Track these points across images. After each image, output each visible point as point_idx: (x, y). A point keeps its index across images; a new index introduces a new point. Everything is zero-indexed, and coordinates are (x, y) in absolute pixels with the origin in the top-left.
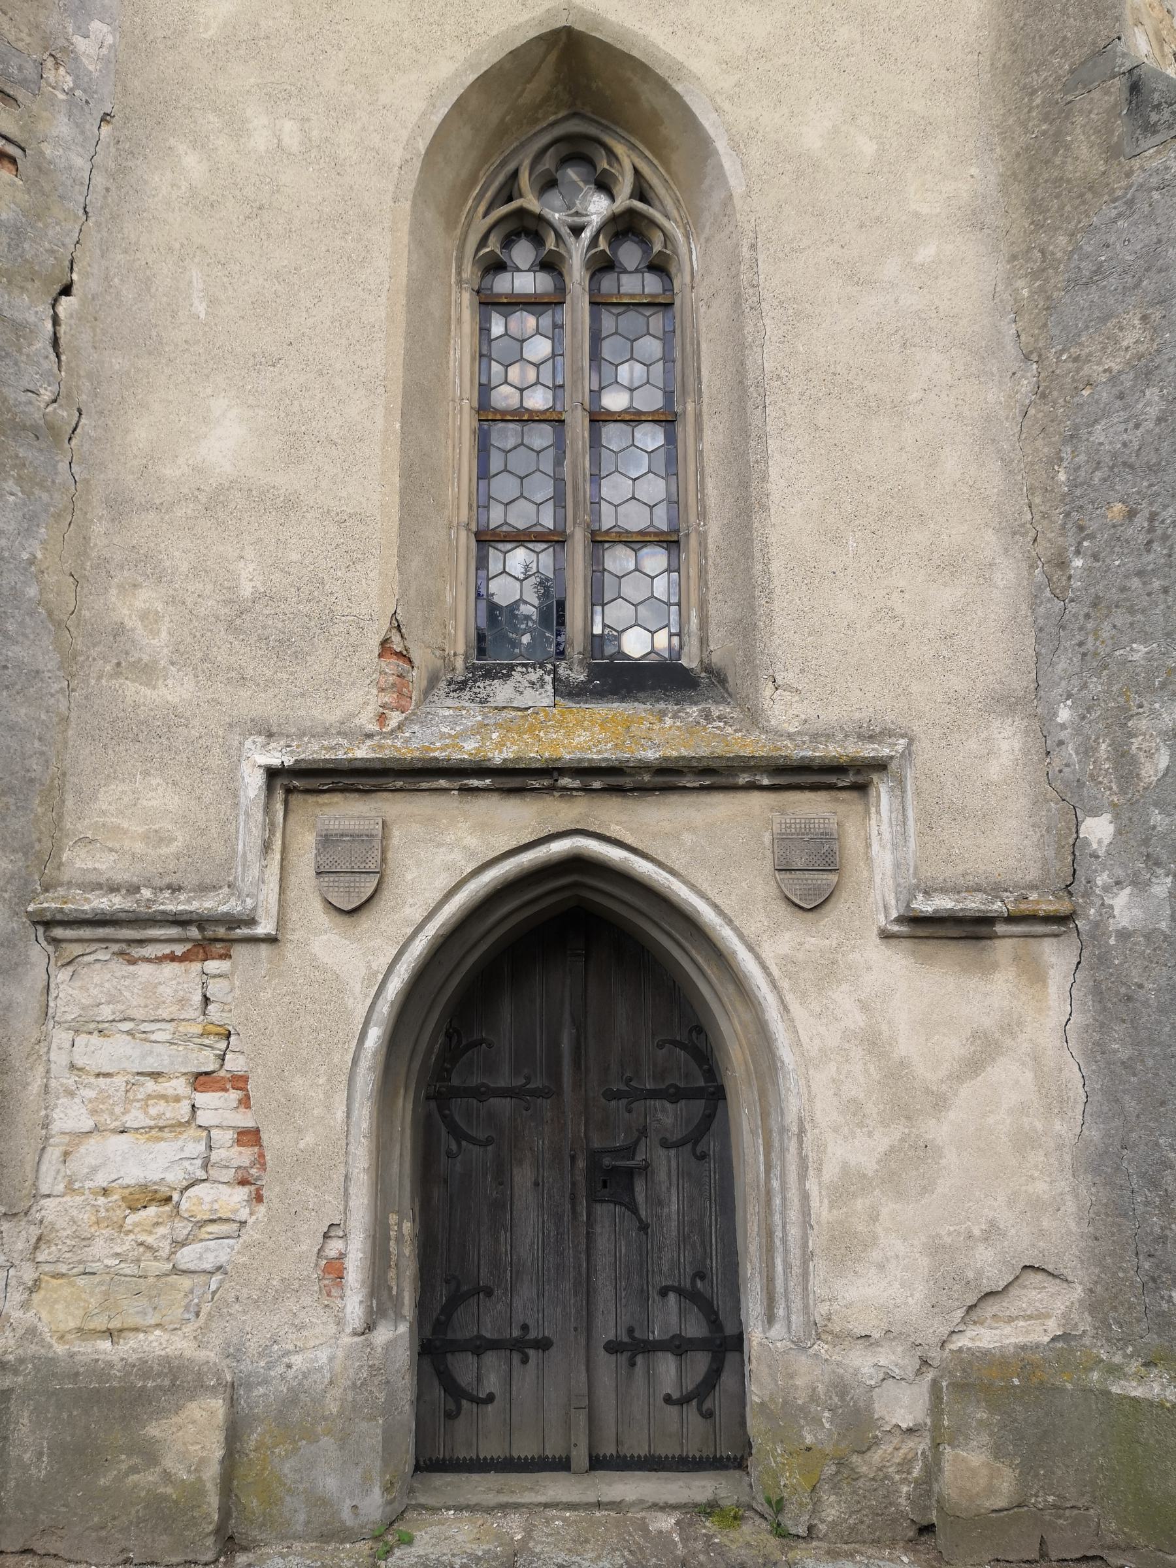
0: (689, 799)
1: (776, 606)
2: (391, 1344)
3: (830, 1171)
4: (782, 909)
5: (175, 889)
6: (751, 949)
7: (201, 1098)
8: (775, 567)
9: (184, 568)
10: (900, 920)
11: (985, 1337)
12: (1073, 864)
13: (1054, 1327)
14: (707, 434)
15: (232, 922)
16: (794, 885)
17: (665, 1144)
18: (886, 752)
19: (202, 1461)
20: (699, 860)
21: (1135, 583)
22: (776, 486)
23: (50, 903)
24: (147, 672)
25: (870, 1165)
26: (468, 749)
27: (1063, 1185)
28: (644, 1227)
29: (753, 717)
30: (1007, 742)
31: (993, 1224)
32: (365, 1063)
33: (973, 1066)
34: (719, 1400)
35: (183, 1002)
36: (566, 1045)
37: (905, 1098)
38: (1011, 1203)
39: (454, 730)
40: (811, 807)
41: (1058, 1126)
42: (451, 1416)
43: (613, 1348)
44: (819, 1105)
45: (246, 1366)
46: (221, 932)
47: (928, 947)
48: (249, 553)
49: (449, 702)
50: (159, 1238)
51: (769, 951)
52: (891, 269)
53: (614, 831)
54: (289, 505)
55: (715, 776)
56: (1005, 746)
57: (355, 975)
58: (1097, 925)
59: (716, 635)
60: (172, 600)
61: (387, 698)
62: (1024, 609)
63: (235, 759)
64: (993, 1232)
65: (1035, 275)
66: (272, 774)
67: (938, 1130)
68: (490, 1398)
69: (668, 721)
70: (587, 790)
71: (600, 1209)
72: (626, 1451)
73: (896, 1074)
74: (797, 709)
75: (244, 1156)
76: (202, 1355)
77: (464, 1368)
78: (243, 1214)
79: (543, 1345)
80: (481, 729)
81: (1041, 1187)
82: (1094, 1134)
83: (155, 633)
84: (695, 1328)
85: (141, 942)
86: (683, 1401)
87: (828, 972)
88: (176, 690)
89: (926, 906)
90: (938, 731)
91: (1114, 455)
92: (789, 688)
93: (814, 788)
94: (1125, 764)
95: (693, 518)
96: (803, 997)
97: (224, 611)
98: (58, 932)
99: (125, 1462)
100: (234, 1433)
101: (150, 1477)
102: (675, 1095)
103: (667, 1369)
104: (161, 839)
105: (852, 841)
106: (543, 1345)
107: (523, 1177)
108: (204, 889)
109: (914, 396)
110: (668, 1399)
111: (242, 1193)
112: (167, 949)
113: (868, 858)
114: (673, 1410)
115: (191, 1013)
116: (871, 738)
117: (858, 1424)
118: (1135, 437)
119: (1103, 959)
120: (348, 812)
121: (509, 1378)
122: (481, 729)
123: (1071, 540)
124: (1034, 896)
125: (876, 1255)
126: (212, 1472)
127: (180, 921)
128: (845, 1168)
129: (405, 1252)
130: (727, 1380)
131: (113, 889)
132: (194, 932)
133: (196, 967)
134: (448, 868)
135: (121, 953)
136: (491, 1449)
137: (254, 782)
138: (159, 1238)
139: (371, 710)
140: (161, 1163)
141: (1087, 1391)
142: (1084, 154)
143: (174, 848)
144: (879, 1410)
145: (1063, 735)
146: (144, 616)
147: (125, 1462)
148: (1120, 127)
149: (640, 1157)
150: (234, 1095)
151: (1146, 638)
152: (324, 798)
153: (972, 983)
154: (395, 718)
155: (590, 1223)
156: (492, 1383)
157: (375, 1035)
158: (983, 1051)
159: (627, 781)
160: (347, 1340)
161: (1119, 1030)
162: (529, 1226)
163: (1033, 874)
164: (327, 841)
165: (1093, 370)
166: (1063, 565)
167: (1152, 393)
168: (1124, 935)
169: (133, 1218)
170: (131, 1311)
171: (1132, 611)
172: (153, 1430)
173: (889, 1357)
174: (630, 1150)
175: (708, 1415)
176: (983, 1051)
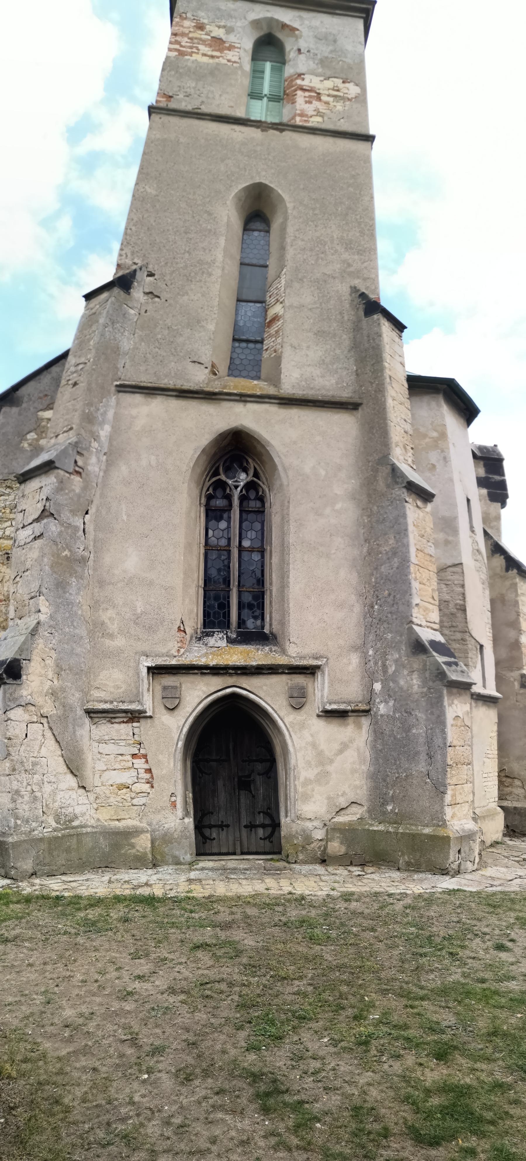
0: (265, 676)
1: (291, 618)
2: (189, 823)
3: (302, 779)
4: (290, 709)
5: (123, 702)
6: (282, 720)
7: (135, 761)
8: (291, 605)
9: (121, 603)
10: (322, 712)
11: (341, 819)
12: (370, 697)
13: (358, 816)
14: (273, 557)
15: (140, 712)
16: (293, 702)
17: (259, 774)
18: (320, 663)
19: (146, 848)
20: (269, 694)
21: (389, 615)
22: (292, 579)
23: (90, 706)
24: (111, 636)
25: (312, 777)
26: (203, 661)
27: (363, 782)
28: (253, 796)
29: (284, 652)
30: (355, 659)
31: (344, 792)
32: (178, 752)
33: (341, 752)
34: (274, 839)
35: (127, 735)
36: (231, 747)
37: (322, 760)
38: (349, 787)
39: (198, 655)
40: (299, 680)
41: (363, 767)
42: (204, 843)
43: (246, 827)
44: (299, 762)
45: (153, 827)
46: (137, 715)
47: (329, 719)
48: (140, 598)
49: (196, 645)
50: (128, 797)
51: (286, 720)
52: (328, 511)
53: (244, 686)
54: (151, 583)
55: (272, 670)
56: (354, 661)
57: (172, 728)
58: (375, 713)
59: (275, 623)
60: (118, 614)
61: (179, 645)
62: (362, 620)
63: (138, 663)
64: (344, 794)
65: (369, 516)
66: (149, 669)
67: (330, 768)
68: (214, 839)
69: (260, 652)
70: (237, 674)
71: (242, 792)
72: (250, 850)
73: (320, 753)
74: (296, 649)
75: (148, 776)
76: (142, 825)
77: (207, 832)
78: (149, 791)
79: (228, 826)
80: (206, 655)
81: (357, 783)
82: (372, 769)
83: (113, 624)
84: (268, 821)
85: (115, 718)
86: (265, 839)
87: (302, 726)
88: (120, 642)
89: (329, 707)
90: (335, 657)
91: (386, 576)
92: (294, 643)
93: (300, 673)
94: (385, 667)
95: (268, 585)
96: (295, 733)
97: (133, 617)
98: (92, 715)
99: (127, 848)
100: (153, 842)
101: (134, 851)
102: (261, 761)
103: (261, 832)
104: (118, 688)
105: (310, 689)
106: (228, 826)
107: (220, 783)
108: (131, 702)
109: (333, 552)
110: (261, 839)
111: (148, 785)
112: (122, 720)
113: (314, 694)
114: (262, 841)
115: (130, 738)
116: (317, 658)
117: (308, 839)
118: (391, 571)
119: (377, 723)
120: (169, 680)
121: (219, 834)
122: (206, 655)
123: (374, 600)
124: (360, 705)
125: (313, 799)
126: (149, 849)
127: (125, 711)
128: (306, 779)
129: (190, 801)
130: (276, 833)
131: (106, 702)
132: (130, 715)
133: (130, 725)
134: (198, 696)
135: (109, 721)
136: (215, 850)
137: (145, 670)
138: (128, 797)
139: (176, 648)
140: (126, 777)
141: (364, 830)
142: (381, 485)
143: (121, 690)
144: (313, 835)
145: (370, 658)
146: (110, 619)
147: (127, 848)
148: (390, 480)
149: (252, 778)
150: (143, 760)
151: (391, 632)
152: (163, 676)
153: (342, 729)
154: (182, 651)
155: (239, 795)
156: (214, 835)
157: (181, 744)
158: (344, 747)
159: (248, 671)
160: (178, 821)
161: (380, 741)
162: (222, 797)
163: (360, 699)
164: (165, 688)
165: (382, 549)
166: (373, 607)
167: (396, 560)
168: (382, 716)
169: (120, 792)
170: (122, 815)
171: (388, 623)
172: (133, 841)
173: (316, 823)
174: (249, 776)
175: (272, 842)
176: (344, 747)
